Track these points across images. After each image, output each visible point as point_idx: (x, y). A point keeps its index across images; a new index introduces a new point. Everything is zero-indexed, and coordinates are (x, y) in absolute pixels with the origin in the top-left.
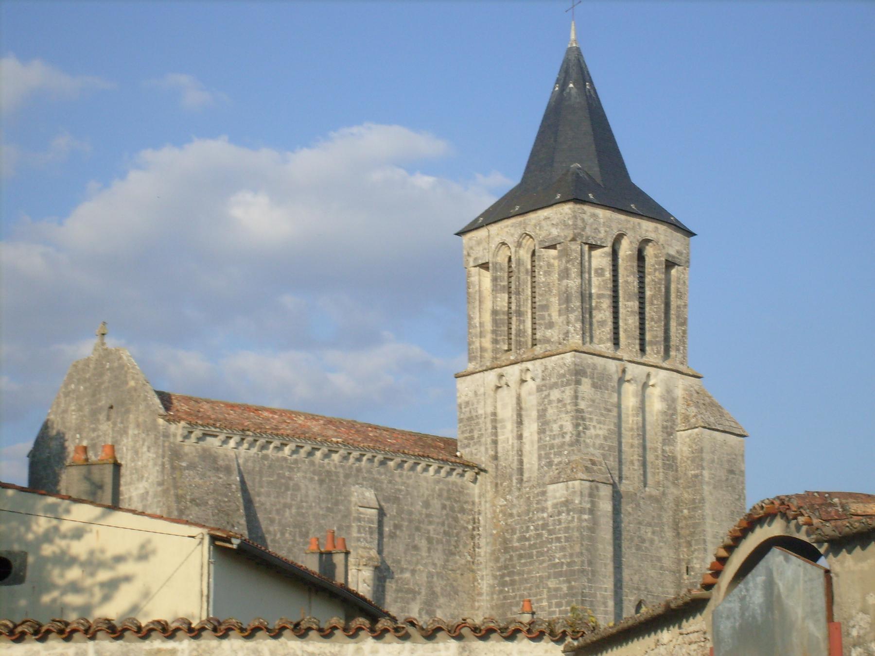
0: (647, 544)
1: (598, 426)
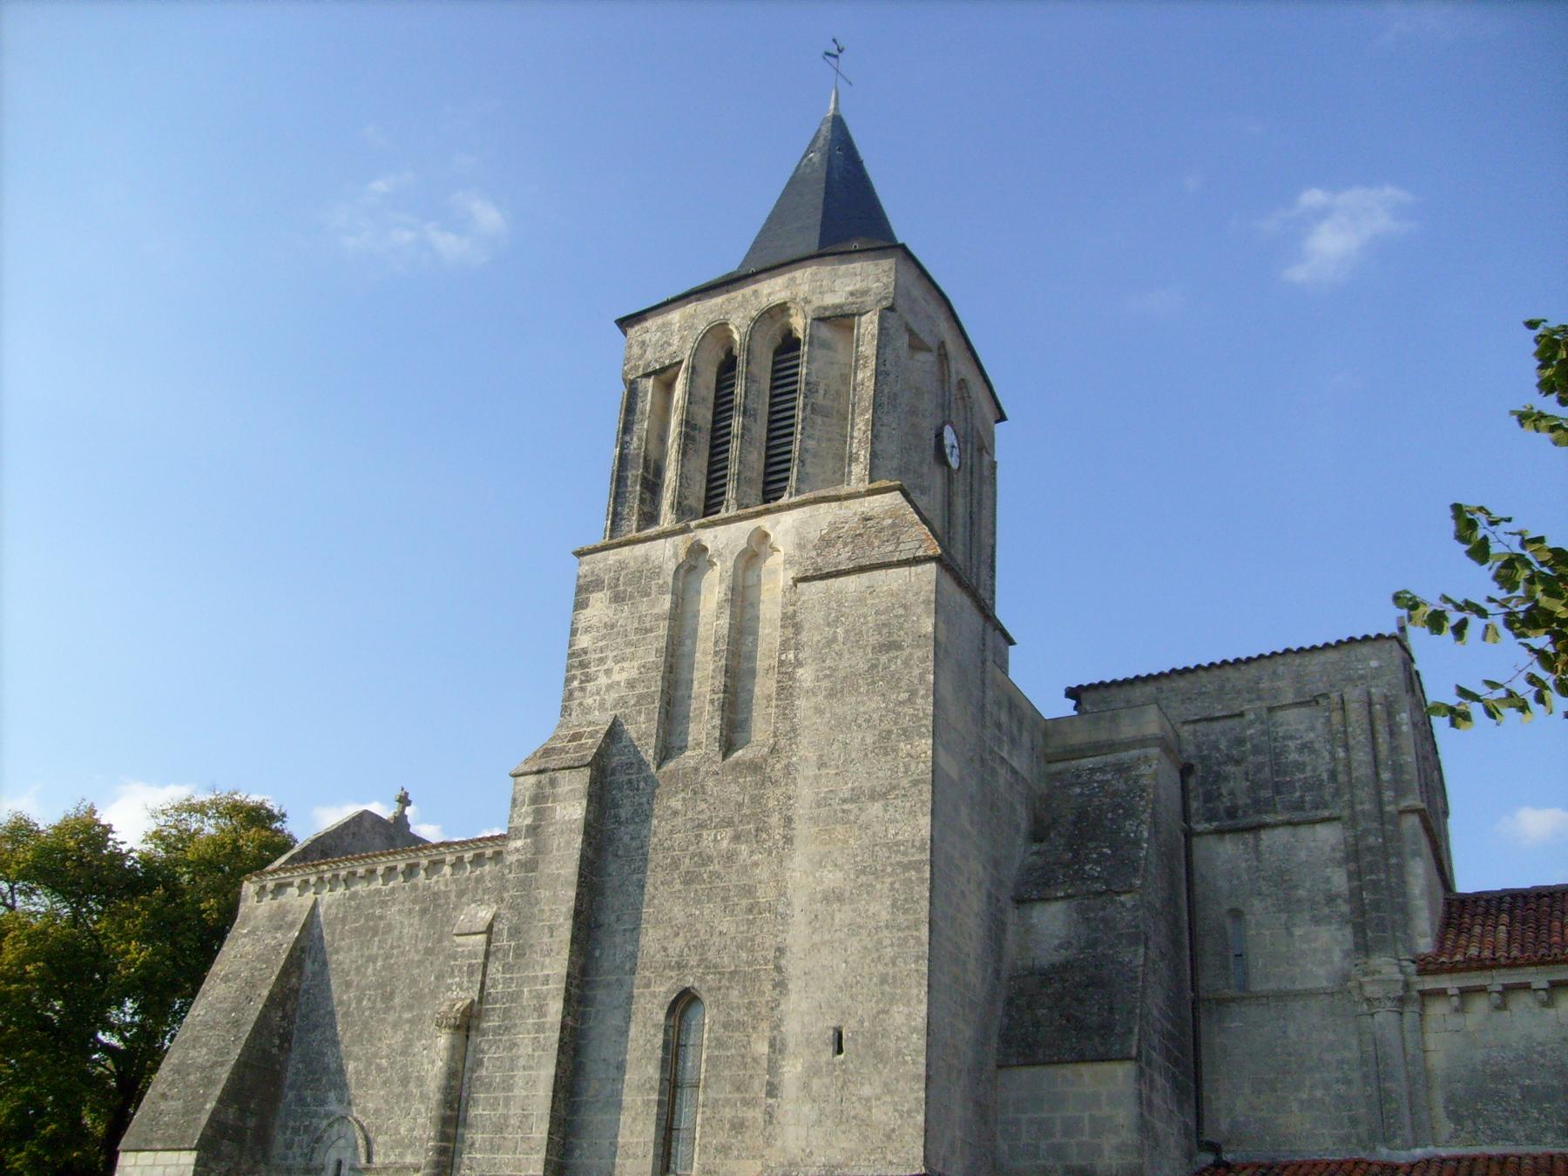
0: (715, 867)
1: (617, 668)
